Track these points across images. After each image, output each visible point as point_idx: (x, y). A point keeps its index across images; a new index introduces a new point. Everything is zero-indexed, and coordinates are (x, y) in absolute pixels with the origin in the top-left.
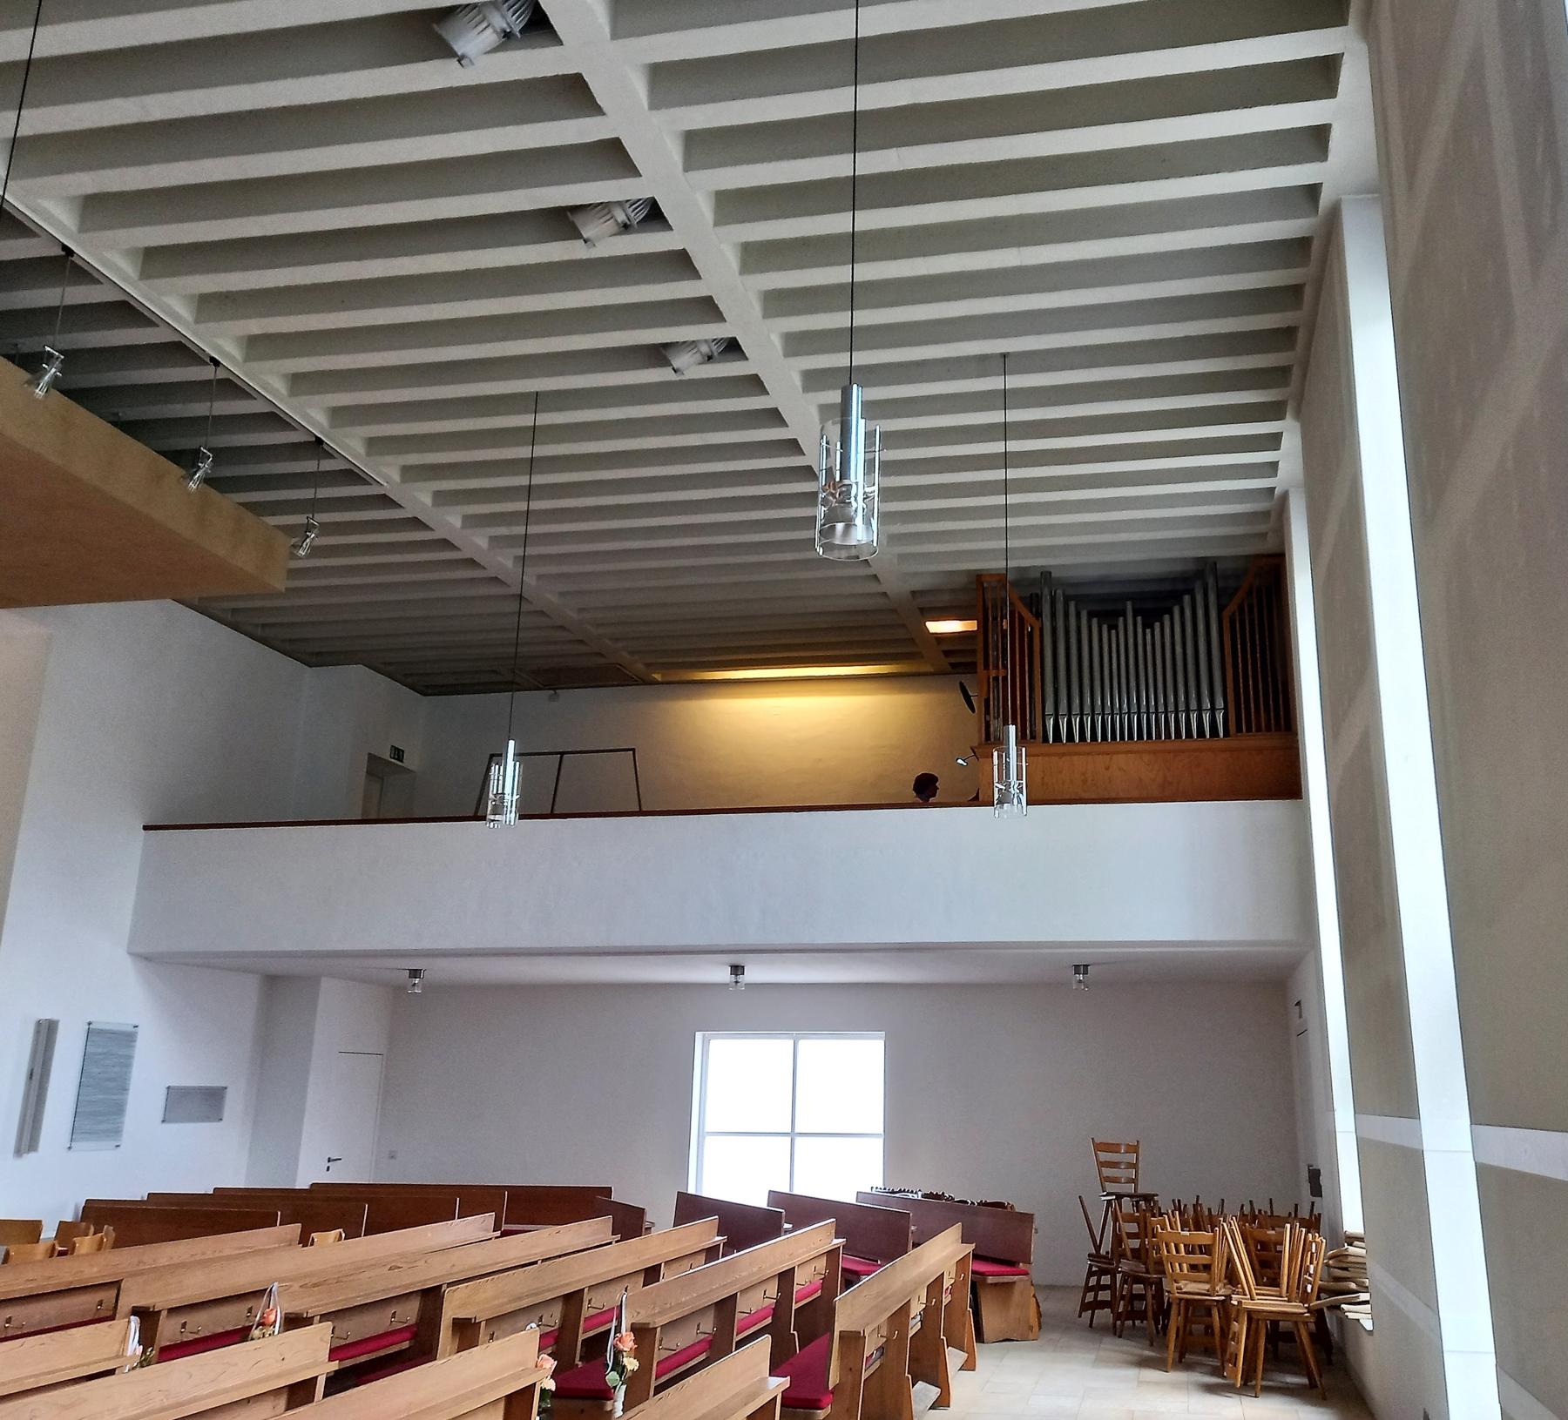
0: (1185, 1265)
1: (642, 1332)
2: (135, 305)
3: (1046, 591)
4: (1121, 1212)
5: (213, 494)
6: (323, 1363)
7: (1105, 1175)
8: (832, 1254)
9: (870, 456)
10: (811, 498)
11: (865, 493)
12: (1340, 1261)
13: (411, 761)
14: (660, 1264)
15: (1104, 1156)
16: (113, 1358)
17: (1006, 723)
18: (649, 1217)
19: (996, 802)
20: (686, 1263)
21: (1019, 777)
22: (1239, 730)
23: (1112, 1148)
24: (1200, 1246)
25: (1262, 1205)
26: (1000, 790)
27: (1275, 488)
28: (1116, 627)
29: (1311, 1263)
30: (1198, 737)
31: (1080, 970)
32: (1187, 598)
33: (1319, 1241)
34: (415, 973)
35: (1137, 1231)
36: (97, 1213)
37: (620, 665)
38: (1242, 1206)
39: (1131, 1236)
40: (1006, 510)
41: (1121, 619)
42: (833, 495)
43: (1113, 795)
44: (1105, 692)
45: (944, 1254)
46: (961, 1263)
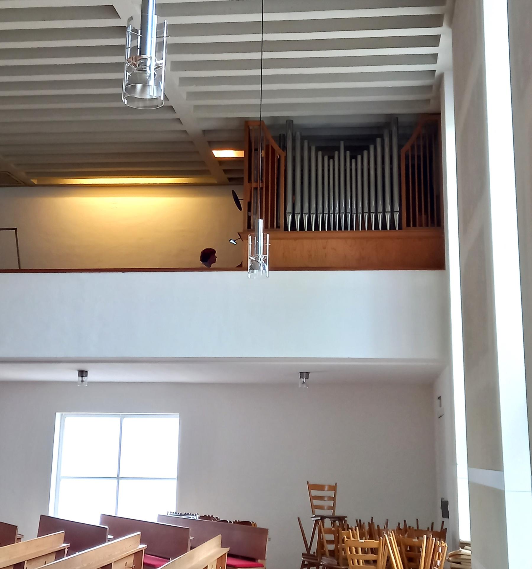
0: (361, 561)
3: (290, 133)
4: (323, 527)
7: (314, 505)
8: (137, 554)
9: (160, 40)
10: (119, 67)
11: (157, 64)
12: (456, 558)
14: (24, 562)
15: (314, 493)
17: (259, 219)
18: (20, 531)
19: (249, 268)
20: (42, 560)
21: (264, 253)
22: (408, 225)
23: (320, 487)
24: (372, 549)
25: (411, 523)
26: (252, 261)
27: (435, 71)
28: (333, 158)
29: (439, 559)
30: (399, 229)
31: (303, 376)
32: (379, 140)
33: (444, 546)
35: (334, 539)
37: (9, 173)
38: (399, 524)
39: (330, 542)
40: (261, 79)
41: (336, 153)
42: (135, 65)
43: (328, 265)
44: (330, 197)
45: (209, 554)
46: (220, 559)
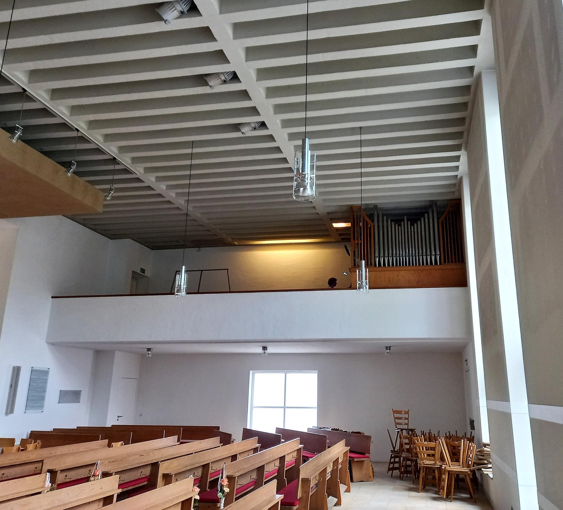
0: (425, 454)
1: (230, 478)
2: (49, 110)
3: (376, 212)
4: (402, 435)
5: (77, 177)
6: (116, 489)
7: (397, 422)
8: (299, 450)
9: (312, 164)
10: (291, 179)
11: (310, 177)
12: (481, 453)
13: (148, 273)
14: (237, 454)
15: (396, 415)
16: (41, 488)
17: (361, 260)
18: (233, 437)
19: (357, 288)
20: (246, 454)
21: (366, 279)
22: (445, 262)
23: (399, 412)
24: (431, 448)
25: (453, 433)
26: (359, 284)
27: (458, 175)
28: (401, 225)
29: (471, 454)
30: (430, 265)
31: (388, 348)
32: (426, 215)
33: (474, 446)
34: (149, 350)
35: (408, 442)
36: (35, 436)
37: (223, 239)
38: (446, 433)
39: (406, 444)
40: (361, 183)
41: (403, 222)
42: (299, 178)
43: (400, 286)
44: (397, 248)
45: (339, 450)
46: (345, 454)
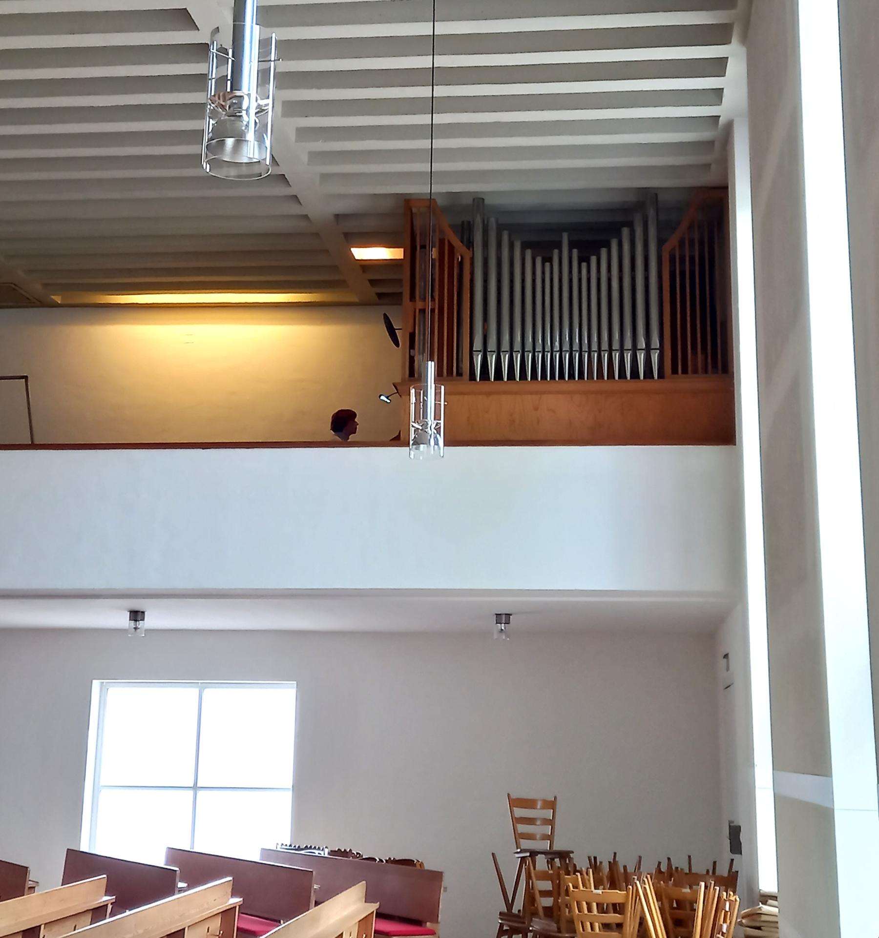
0: (597, 925)
3: (478, 220)
4: (534, 868)
7: (519, 832)
8: (227, 914)
9: (264, 65)
10: (196, 110)
11: (259, 106)
12: (754, 920)
14: (40, 926)
15: (519, 812)
17: (428, 361)
18: (32, 876)
19: (411, 442)
20: (70, 924)
21: (437, 417)
22: (674, 371)
23: (529, 804)
24: (614, 905)
25: (680, 863)
26: (416, 430)
27: (719, 116)
28: (550, 260)
29: (725, 921)
30: (659, 377)
31: (501, 619)
32: (625, 231)
33: (734, 901)
35: (551, 889)
37: (15, 285)
38: (660, 863)
39: (545, 894)
40: (432, 131)
41: (556, 252)
42: (223, 107)
43: (541, 437)
44: (546, 326)
45: (346, 913)
46: (364, 922)
